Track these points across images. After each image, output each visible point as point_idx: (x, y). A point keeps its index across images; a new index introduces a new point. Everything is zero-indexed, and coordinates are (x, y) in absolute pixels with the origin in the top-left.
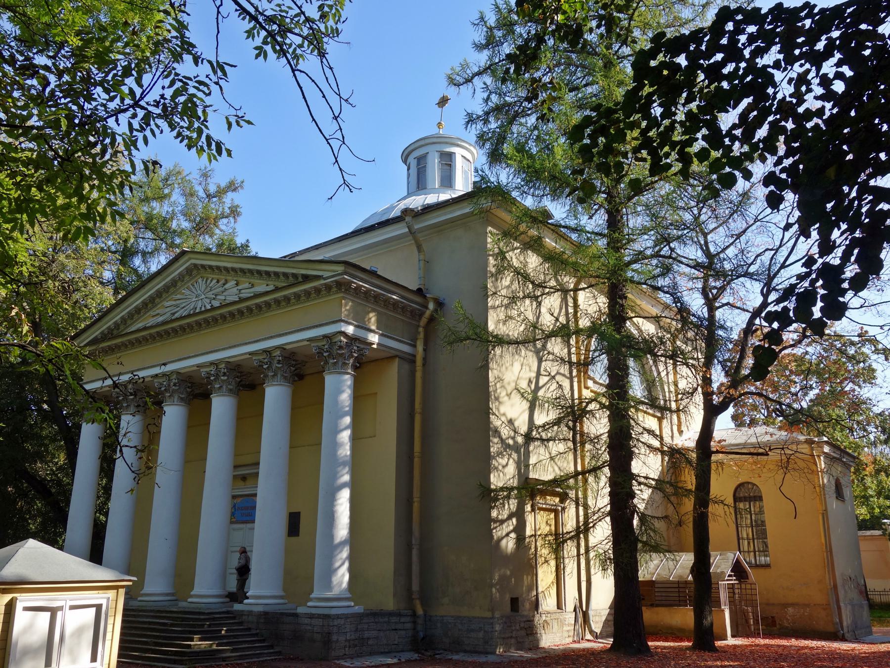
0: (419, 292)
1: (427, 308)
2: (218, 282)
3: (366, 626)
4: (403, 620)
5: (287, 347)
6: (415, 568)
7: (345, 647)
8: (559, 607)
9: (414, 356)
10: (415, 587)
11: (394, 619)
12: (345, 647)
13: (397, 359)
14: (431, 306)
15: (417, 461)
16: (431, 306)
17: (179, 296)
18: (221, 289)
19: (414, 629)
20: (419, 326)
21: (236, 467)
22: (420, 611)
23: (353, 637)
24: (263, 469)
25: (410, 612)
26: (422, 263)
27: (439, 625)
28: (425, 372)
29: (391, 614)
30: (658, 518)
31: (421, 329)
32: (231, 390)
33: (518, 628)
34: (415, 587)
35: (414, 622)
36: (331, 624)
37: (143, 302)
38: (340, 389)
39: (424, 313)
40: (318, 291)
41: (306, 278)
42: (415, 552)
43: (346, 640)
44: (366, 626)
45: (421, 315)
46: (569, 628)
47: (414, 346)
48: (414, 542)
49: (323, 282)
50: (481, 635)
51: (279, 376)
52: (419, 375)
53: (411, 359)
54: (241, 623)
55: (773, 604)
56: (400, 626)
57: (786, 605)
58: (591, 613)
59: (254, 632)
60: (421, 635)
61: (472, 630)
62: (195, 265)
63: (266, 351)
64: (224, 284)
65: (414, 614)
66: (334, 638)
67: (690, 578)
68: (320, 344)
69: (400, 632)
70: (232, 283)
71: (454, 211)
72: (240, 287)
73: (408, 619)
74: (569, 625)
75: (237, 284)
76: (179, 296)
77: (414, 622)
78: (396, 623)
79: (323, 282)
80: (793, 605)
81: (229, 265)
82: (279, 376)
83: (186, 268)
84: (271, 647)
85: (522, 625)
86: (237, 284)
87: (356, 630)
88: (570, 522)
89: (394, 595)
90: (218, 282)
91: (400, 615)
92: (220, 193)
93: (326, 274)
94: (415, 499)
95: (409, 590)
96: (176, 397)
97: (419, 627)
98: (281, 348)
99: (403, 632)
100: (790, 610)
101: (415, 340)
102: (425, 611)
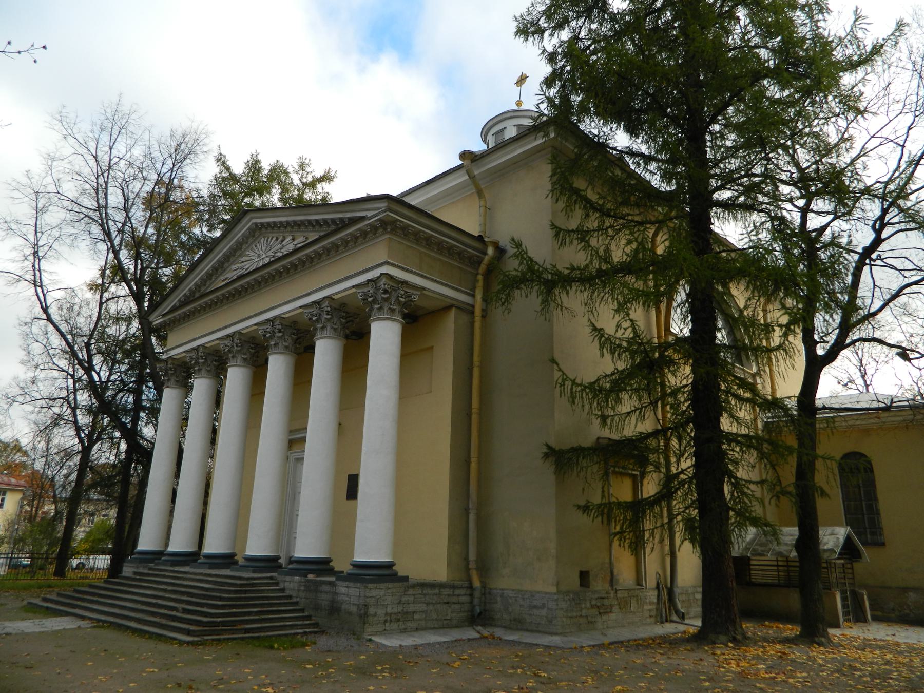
0: (480, 238)
1: (485, 254)
2: (277, 239)
3: (411, 598)
4: (457, 592)
5: (336, 297)
6: (472, 534)
7: (386, 621)
8: (639, 583)
9: (473, 306)
10: (472, 556)
11: (446, 592)
12: (386, 621)
13: (453, 311)
14: (490, 251)
15: (474, 417)
16: (490, 251)
17: (244, 259)
18: (280, 246)
19: (471, 603)
20: (478, 274)
21: (291, 432)
22: (477, 583)
23: (395, 610)
24: (309, 434)
25: (466, 584)
26: (482, 209)
27: (499, 599)
28: (484, 327)
29: (442, 586)
30: (754, 483)
31: (480, 277)
32: (286, 347)
33: (588, 605)
34: (472, 556)
35: (471, 595)
36: (368, 595)
37: (212, 267)
38: (384, 336)
39: (482, 260)
40: (364, 234)
41: (354, 221)
42: (472, 517)
43: (386, 614)
44: (411, 598)
45: (480, 263)
46: (650, 607)
47: (473, 296)
48: (470, 506)
49: (367, 222)
50: (544, 612)
51: (329, 328)
52: (477, 325)
53: (469, 310)
54: (283, 590)
55: (890, 588)
56: (454, 599)
57: (905, 590)
58: (677, 591)
59: (295, 600)
60: (478, 610)
61: (535, 607)
62: (256, 224)
63: (317, 303)
64: (282, 241)
65: (471, 587)
66: (372, 611)
67: (794, 554)
68: (365, 290)
69: (453, 606)
70: (289, 238)
71: (515, 149)
72: (295, 242)
73: (463, 592)
74: (651, 603)
75: (293, 239)
76: (244, 259)
77: (471, 595)
78: (449, 595)
79: (367, 222)
80: (915, 589)
81: (283, 219)
82: (329, 328)
83: (249, 229)
84: (309, 617)
85: (594, 602)
86: (293, 239)
87: (400, 603)
88: (650, 488)
89: (448, 565)
90: (277, 239)
91: (454, 587)
92: (312, 185)
93: (369, 214)
94: (473, 460)
95: (466, 559)
96: (239, 358)
97: (476, 601)
98: (329, 298)
99: (456, 606)
100: (912, 596)
101: (474, 289)
102: (481, 582)
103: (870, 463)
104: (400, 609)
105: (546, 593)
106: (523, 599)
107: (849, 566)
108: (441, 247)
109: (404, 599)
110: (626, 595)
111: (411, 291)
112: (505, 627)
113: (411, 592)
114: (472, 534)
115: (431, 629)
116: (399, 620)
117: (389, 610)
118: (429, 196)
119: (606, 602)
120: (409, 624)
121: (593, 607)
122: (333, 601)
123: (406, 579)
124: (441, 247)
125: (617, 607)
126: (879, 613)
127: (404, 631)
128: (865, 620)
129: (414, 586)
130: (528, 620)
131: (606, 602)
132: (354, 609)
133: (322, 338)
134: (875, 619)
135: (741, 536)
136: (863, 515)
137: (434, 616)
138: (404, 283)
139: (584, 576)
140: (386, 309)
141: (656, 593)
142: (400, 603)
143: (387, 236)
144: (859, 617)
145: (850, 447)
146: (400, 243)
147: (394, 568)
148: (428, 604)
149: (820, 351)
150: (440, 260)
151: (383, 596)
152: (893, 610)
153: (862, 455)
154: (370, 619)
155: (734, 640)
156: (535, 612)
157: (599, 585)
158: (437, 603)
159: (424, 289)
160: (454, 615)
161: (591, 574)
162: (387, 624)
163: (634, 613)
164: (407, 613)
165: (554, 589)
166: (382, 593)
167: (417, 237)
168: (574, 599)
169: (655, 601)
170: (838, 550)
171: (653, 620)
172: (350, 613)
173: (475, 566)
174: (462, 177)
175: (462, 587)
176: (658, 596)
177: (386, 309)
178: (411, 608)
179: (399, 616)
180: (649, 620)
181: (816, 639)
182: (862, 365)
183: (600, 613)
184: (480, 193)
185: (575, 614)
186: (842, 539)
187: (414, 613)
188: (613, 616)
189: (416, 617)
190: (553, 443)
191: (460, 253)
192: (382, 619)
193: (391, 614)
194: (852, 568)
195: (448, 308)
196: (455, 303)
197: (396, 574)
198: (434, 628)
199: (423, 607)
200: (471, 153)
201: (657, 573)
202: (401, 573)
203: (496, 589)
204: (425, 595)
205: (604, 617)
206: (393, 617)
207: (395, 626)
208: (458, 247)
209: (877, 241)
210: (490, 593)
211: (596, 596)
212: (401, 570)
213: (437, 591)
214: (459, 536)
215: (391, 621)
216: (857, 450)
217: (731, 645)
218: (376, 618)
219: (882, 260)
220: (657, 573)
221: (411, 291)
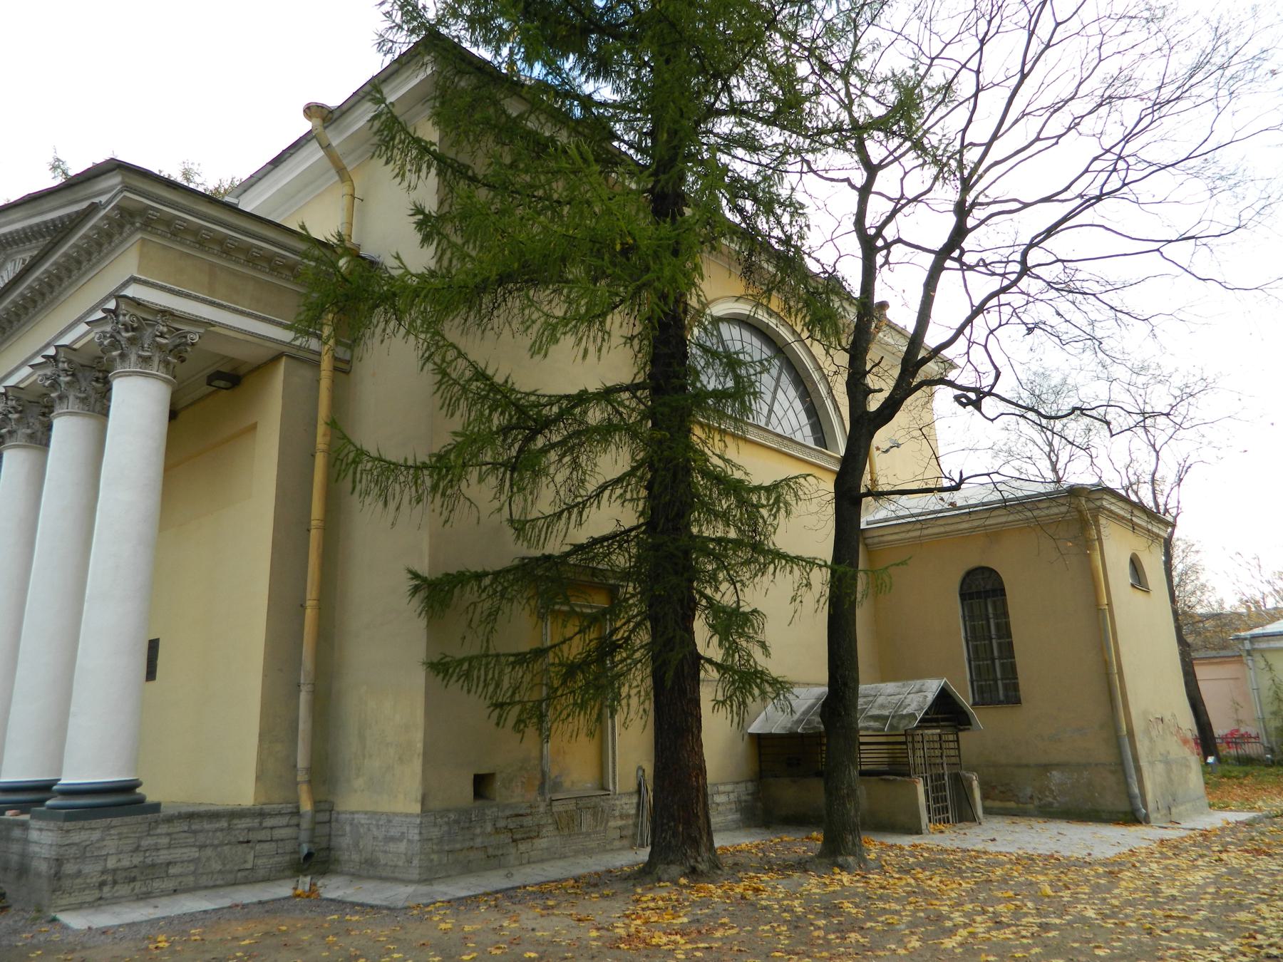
3: (165, 841)
4: (269, 822)
23: (126, 863)
27: (348, 828)
33: (489, 828)
34: (302, 761)
51: (71, 398)
55: (1027, 766)
57: (1046, 768)
65: (297, 813)
69: (258, 847)
73: (283, 821)
78: (249, 830)
85: (501, 824)
87: (137, 849)
89: (258, 778)
93: (103, 199)
100: (1056, 775)
103: (1002, 583)
104: (137, 860)
105: (407, 815)
106: (378, 826)
107: (951, 737)
108: (253, 258)
109: (145, 843)
110: (572, 806)
111: (186, 328)
112: (353, 875)
113: (163, 829)
114: (304, 725)
115: (206, 888)
116: (134, 879)
117: (111, 863)
118: (280, 186)
119: (528, 821)
120: (156, 884)
121: (497, 831)
122: (23, 855)
123: (156, 807)
124: (253, 258)
125: (551, 828)
126: (997, 804)
127: (145, 897)
128: (973, 819)
129: (170, 820)
130: (383, 862)
131: (528, 821)
132: (43, 867)
133: (64, 414)
134: (988, 812)
135: (744, 702)
136: (993, 660)
137: (216, 866)
138: (166, 313)
139: (482, 784)
140: (133, 358)
141: (635, 800)
142: (137, 849)
143: (139, 236)
144: (964, 814)
145: (974, 561)
146: (164, 247)
147: (138, 790)
148: (202, 847)
149: (874, 404)
150: (254, 278)
151: (111, 842)
152: (1031, 798)
153: (992, 571)
154: (66, 883)
155: (693, 873)
156: (392, 847)
157: (513, 795)
158: (222, 844)
159: (210, 323)
160: (259, 862)
161: (498, 777)
162: (106, 889)
163: (588, 834)
164: (153, 865)
165: (417, 808)
166: (96, 835)
167: (201, 240)
168: (457, 822)
169: (633, 812)
170: (920, 716)
171: (626, 842)
172: (39, 875)
173: (306, 778)
174: (313, 154)
175: (280, 814)
176: (638, 804)
177: (133, 358)
178: (164, 856)
179: (135, 873)
180: (617, 844)
181: (840, 860)
182: (1052, 450)
183: (514, 841)
184: (342, 172)
185: (458, 846)
186: (930, 697)
187: (169, 864)
188: (542, 843)
189: (172, 871)
190: (424, 569)
191: (292, 268)
192: (95, 880)
193: (115, 871)
194: (958, 741)
195: (276, 358)
196: (285, 349)
197: (141, 800)
198: (215, 886)
199: (194, 853)
200: (321, 107)
201: (640, 768)
202: (151, 798)
203: (345, 812)
204: (195, 832)
205: (523, 847)
206: (120, 875)
207: (123, 890)
208: (284, 257)
209: (960, 232)
210: (337, 821)
211: (508, 812)
212: (150, 793)
213: (223, 824)
214: (276, 728)
215: (115, 883)
216: (984, 564)
217: (683, 881)
218: (79, 881)
219: (986, 265)
220: (640, 768)
221: (186, 328)
